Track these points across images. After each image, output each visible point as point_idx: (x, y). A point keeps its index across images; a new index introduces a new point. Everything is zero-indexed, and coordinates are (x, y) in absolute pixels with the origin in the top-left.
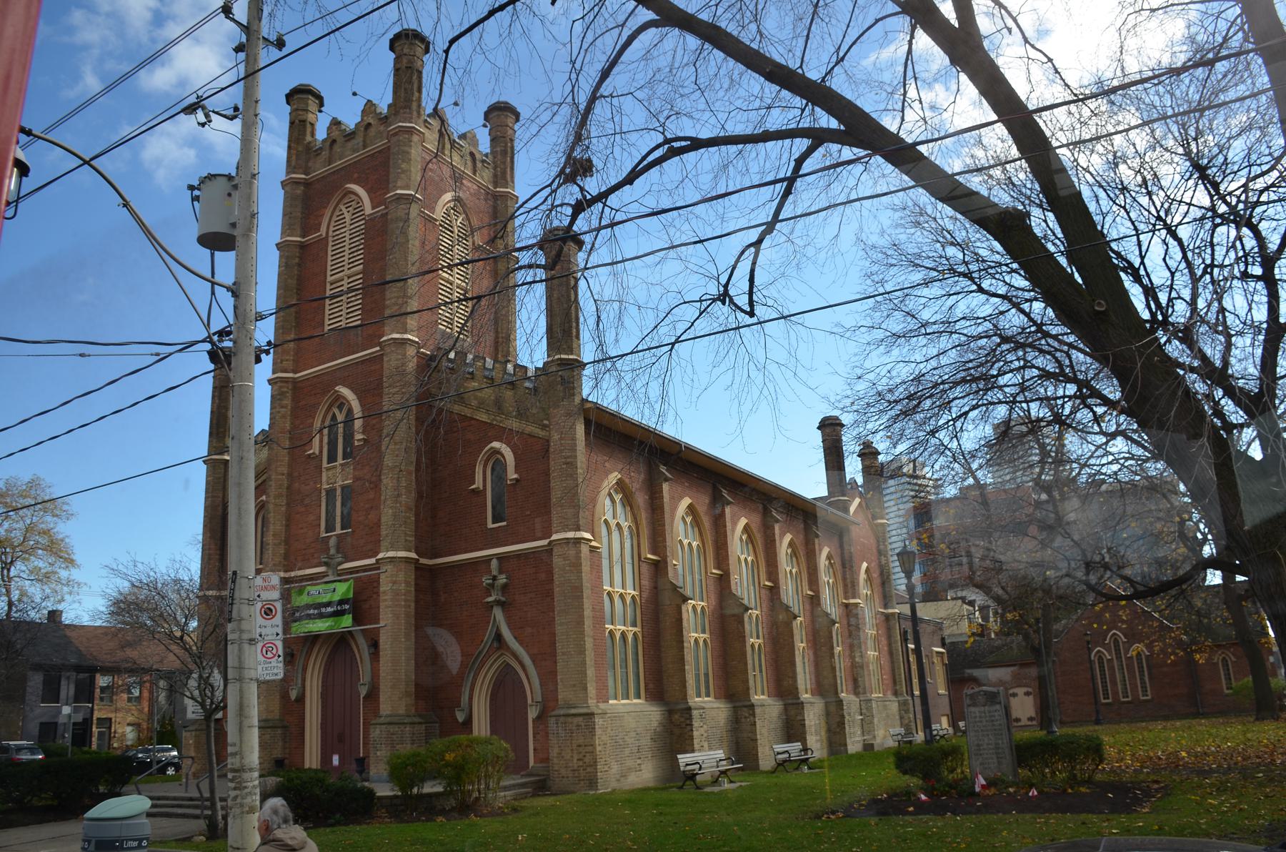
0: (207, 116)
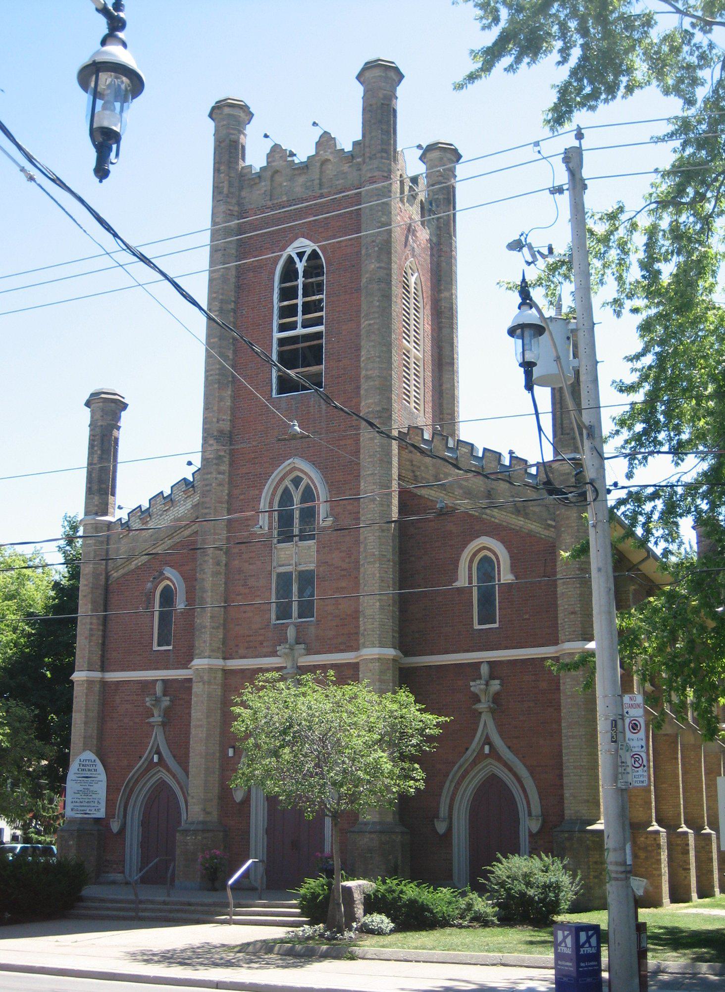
0: (533, 256)
